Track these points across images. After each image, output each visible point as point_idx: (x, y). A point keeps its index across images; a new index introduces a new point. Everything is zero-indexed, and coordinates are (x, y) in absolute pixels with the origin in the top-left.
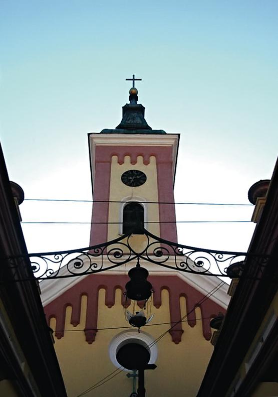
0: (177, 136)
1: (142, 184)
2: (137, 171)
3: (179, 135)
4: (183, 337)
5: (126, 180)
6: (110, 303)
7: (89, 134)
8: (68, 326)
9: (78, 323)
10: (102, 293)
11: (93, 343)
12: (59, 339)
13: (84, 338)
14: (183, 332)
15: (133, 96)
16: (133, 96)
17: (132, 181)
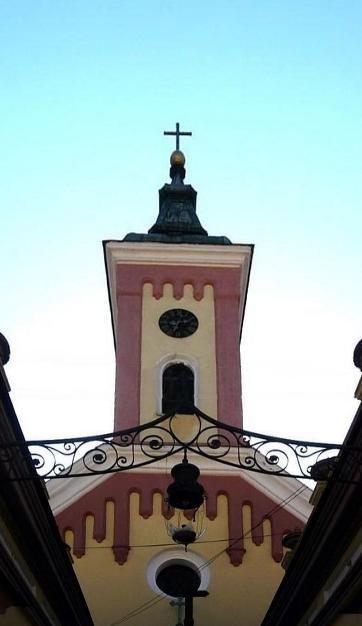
0: (250, 248)
3: (252, 246)
4: (246, 558)
6: (146, 513)
7: (105, 243)
8: (90, 542)
10: (135, 498)
13: (112, 557)
14: (245, 551)
15: (178, 168)
16: (178, 168)
17: (176, 328)
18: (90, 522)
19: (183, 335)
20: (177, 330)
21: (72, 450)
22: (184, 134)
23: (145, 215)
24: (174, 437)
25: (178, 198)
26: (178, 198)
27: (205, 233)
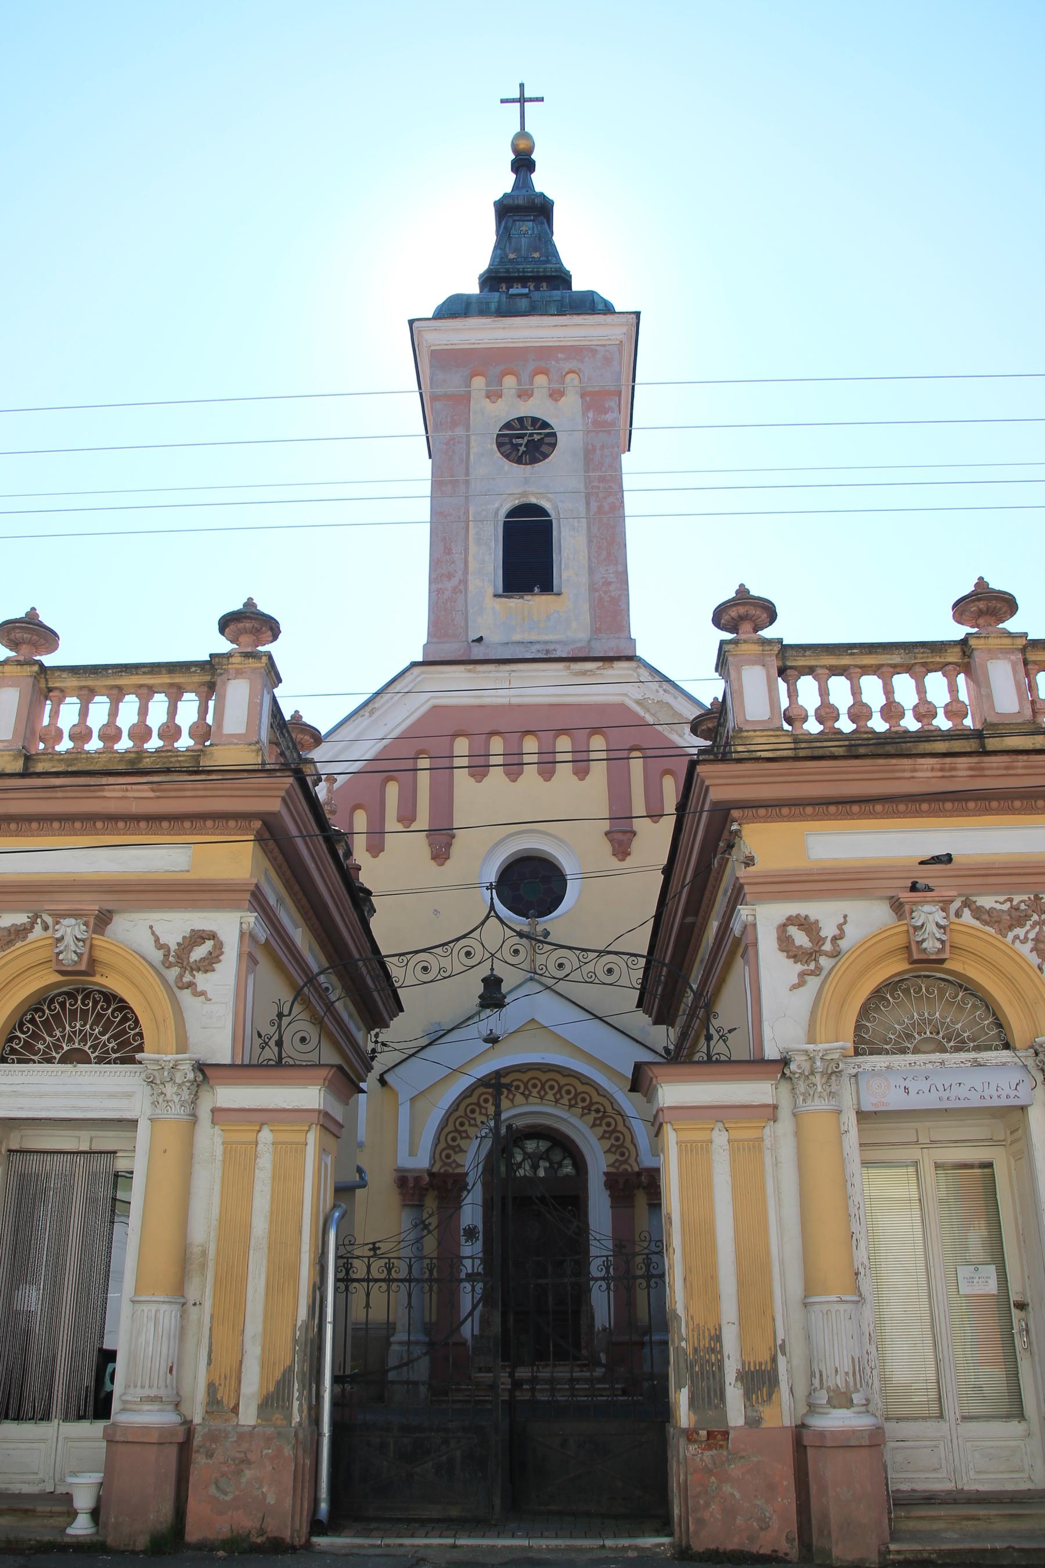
0: (634, 316)
1: (546, 456)
2: (535, 420)
3: (638, 314)
4: (636, 845)
5: (509, 446)
6: (479, 769)
7: (411, 322)
9: (413, 819)
11: (448, 862)
12: (374, 857)
13: (426, 852)
14: (634, 833)
15: (523, 163)
16: (523, 163)
17: (522, 449)
18: (392, 791)
19: (534, 461)
20: (524, 452)
21: (405, 962)
22: (531, 100)
23: (466, 253)
24: (487, 917)
25: (524, 214)
26: (524, 214)
27: (563, 279)
